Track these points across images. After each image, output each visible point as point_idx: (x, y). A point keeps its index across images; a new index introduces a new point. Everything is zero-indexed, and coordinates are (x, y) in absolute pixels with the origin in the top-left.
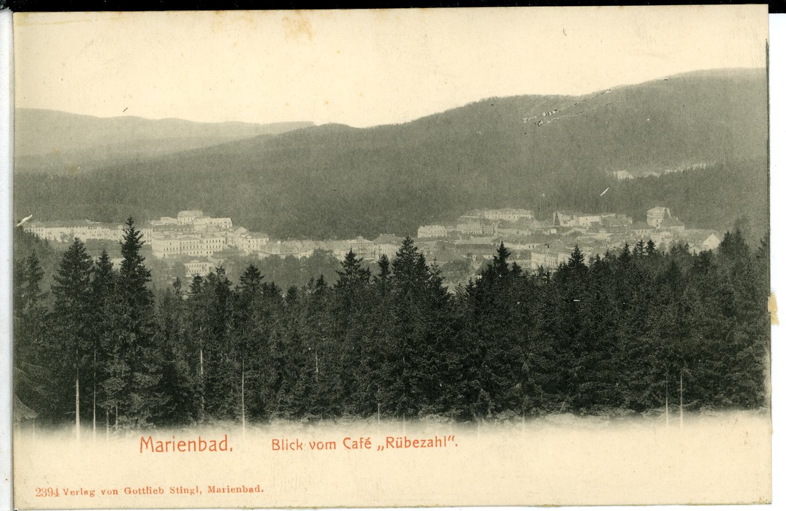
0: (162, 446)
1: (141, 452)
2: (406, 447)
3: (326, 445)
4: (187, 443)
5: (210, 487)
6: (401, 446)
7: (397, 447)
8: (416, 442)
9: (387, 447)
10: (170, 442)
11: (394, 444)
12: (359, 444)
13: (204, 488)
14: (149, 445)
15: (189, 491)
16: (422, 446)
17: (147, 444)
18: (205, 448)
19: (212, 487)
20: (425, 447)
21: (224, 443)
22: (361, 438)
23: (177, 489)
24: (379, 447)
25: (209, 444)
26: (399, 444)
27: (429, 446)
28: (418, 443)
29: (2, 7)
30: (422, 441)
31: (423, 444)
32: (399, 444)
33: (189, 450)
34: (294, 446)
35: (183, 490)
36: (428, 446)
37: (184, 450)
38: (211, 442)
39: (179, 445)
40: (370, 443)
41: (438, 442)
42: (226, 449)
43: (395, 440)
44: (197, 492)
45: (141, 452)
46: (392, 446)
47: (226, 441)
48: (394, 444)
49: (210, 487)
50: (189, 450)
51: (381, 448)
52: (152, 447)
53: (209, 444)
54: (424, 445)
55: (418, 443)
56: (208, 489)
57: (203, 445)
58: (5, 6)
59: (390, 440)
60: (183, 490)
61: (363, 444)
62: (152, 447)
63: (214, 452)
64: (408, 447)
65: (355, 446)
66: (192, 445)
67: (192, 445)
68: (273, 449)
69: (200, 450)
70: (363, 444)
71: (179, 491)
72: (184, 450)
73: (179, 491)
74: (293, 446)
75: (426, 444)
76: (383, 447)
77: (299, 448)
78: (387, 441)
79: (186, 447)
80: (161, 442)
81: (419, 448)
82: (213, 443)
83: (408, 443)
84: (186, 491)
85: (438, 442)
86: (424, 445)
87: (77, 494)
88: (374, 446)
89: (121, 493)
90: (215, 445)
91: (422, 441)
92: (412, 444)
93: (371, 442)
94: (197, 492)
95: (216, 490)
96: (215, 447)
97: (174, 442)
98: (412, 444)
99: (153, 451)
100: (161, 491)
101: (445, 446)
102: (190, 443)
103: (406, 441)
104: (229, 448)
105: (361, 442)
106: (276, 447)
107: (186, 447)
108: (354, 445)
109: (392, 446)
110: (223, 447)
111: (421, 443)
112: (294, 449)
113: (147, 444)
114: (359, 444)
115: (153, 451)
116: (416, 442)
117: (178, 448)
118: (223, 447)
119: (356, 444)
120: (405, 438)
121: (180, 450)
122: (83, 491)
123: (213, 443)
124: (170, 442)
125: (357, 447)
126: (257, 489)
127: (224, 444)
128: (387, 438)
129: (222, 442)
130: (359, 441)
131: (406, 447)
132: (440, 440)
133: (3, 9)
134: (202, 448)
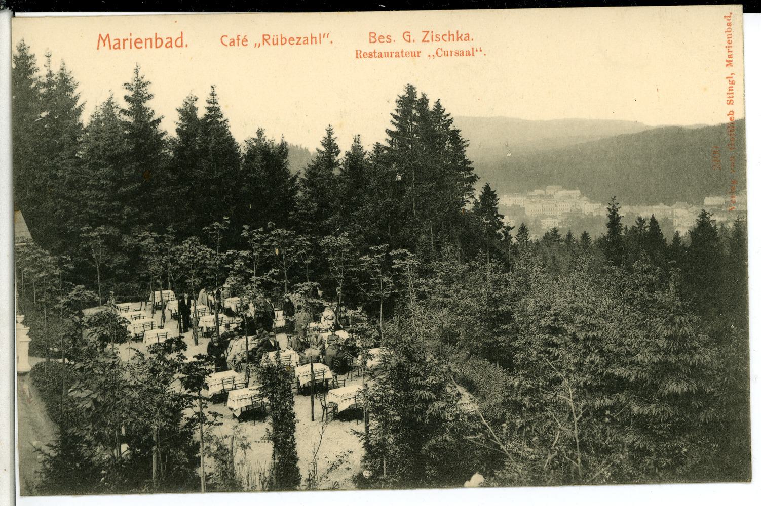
0: (119, 43)
1: (98, 49)
2: (282, 44)
3: (156, 41)
4: (144, 41)
5: (727, 65)
6: (277, 44)
7: (274, 44)
8: (139, 41)
9: (264, 44)
10: (127, 40)
11: (270, 41)
12: (236, 41)
13: (728, 71)
14: (107, 42)
15: (731, 85)
16: (297, 44)
17: (104, 42)
18: (161, 45)
19: (104, 37)
20: (428, 41)
21: (180, 40)
22: (238, 36)
23: (729, 97)
24: (256, 44)
25: (165, 41)
26: (275, 42)
27: (230, 45)
28: (294, 40)
29: (2, 7)
30: (297, 38)
31: (299, 41)
32: (275, 42)
33: (146, 48)
34: (446, 38)
35: (731, 92)
36: (304, 43)
37: (141, 47)
38: (115, 40)
39: (135, 43)
40: (247, 41)
41: (314, 40)
42: (182, 46)
43: (272, 37)
44: (732, 78)
45: (98, 49)
46: (268, 42)
47: (182, 37)
48: (270, 41)
49: (727, 65)
50: (146, 48)
51: (258, 45)
52: (110, 45)
53: (165, 41)
54: (299, 43)
55: (294, 40)
56: (729, 67)
57: (159, 42)
58: (6, 6)
59: (266, 37)
60: (731, 92)
61: (240, 42)
62: (110, 45)
63: (118, 50)
64: (159, 47)
65: (232, 43)
66: (149, 42)
67: (149, 42)
68: (370, 42)
69: (156, 47)
70: (240, 42)
71: (731, 95)
72: (141, 47)
73: (731, 95)
74: (444, 37)
75: (301, 42)
76: (259, 44)
77: (459, 39)
78: (264, 39)
79: (143, 45)
80: (119, 40)
81: (295, 46)
82: (117, 41)
83: (284, 41)
84: (730, 89)
85: (314, 40)
86: (299, 43)
87: (732, 51)
88: (251, 43)
89: (728, 71)
90: (171, 42)
91: (297, 38)
92: (288, 41)
93: (248, 40)
94: (732, 78)
95: (730, 59)
96: (119, 45)
97: (131, 40)
98: (288, 41)
99: (110, 48)
100: (731, 113)
101: (124, 48)
102: (146, 40)
103: (282, 39)
104: (184, 45)
105: (238, 39)
106: (373, 40)
107: (143, 45)
108: (168, 43)
109: (268, 42)
110: (179, 43)
111: (297, 40)
112: (227, 46)
113: (104, 42)
114: (236, 41)
115: (110, 48)
116: (139, 41)
117: (136, 46)
118: (179, 43)
119: (234, 42)
120: (281, 35)
121: (137, 47)
122: (728, 45)
123: (169, 40)
124: (127, 40)
125: (307, 43)
126: (729, 18)
127: (180, 40)
128: (264, 35)
129: (177, 39)
130: (235, 38)
131: (282, 44)
132: (453, 35)
133: (3, 9)
134: (158, 45)
